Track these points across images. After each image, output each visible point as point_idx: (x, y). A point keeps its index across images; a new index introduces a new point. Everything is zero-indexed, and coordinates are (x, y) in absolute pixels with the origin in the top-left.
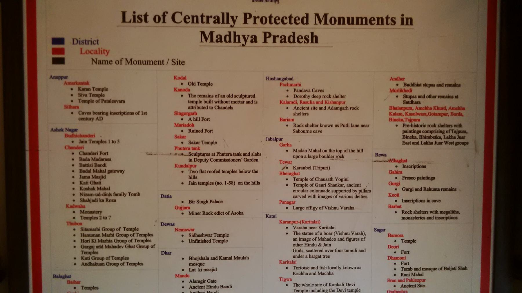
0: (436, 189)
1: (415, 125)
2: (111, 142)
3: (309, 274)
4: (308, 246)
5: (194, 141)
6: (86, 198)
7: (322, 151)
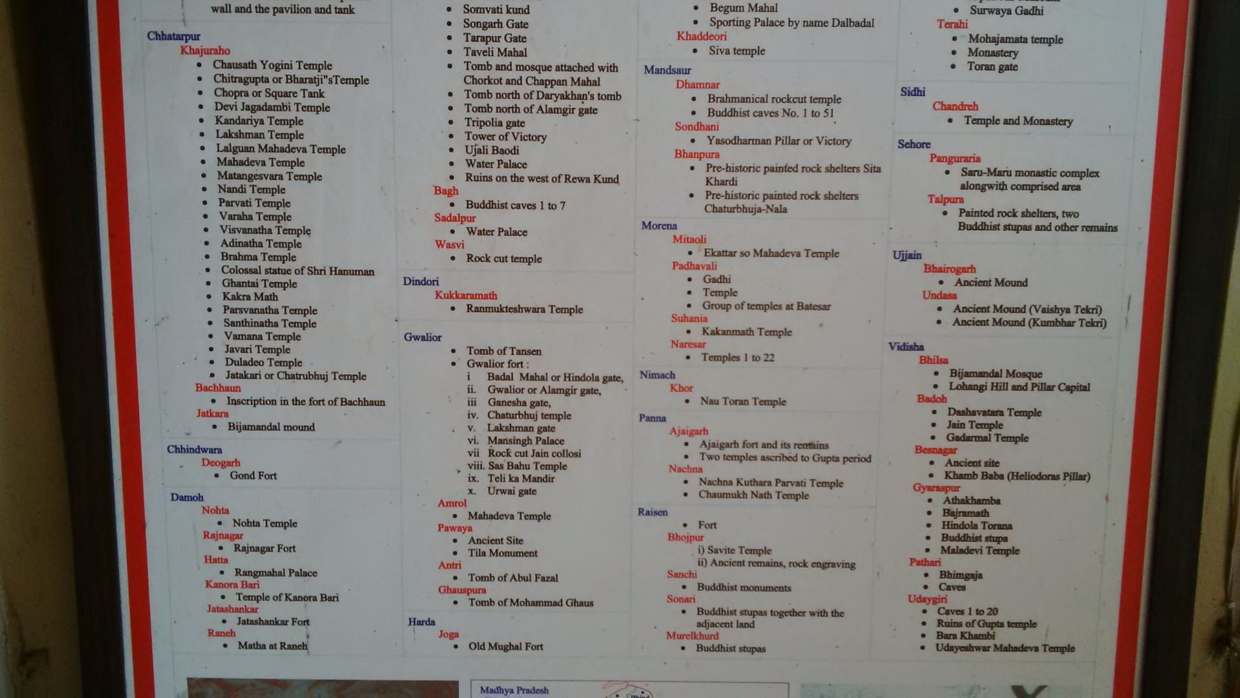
0: (239, 322)
4: (571, 379)
6: (240, 370)
7: (549, 378)
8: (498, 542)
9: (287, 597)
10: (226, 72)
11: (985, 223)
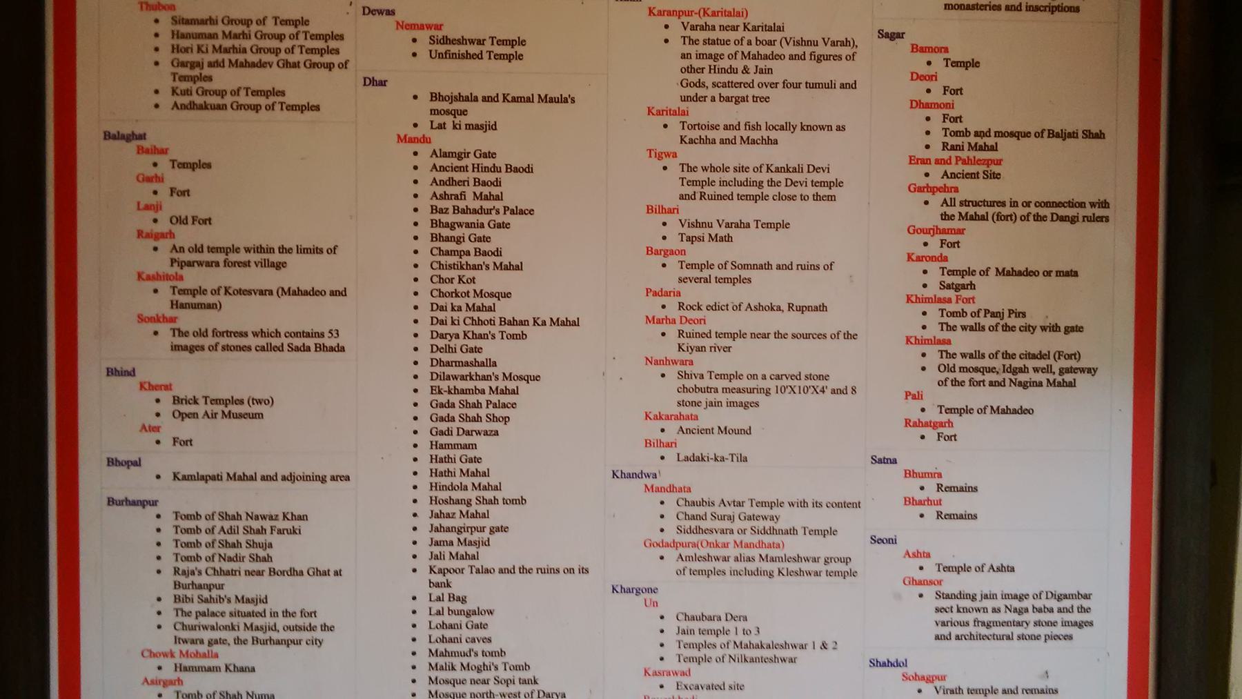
8: (462, 169)
9: (768, 168)
10: (443, 259)
11: (452, 178)
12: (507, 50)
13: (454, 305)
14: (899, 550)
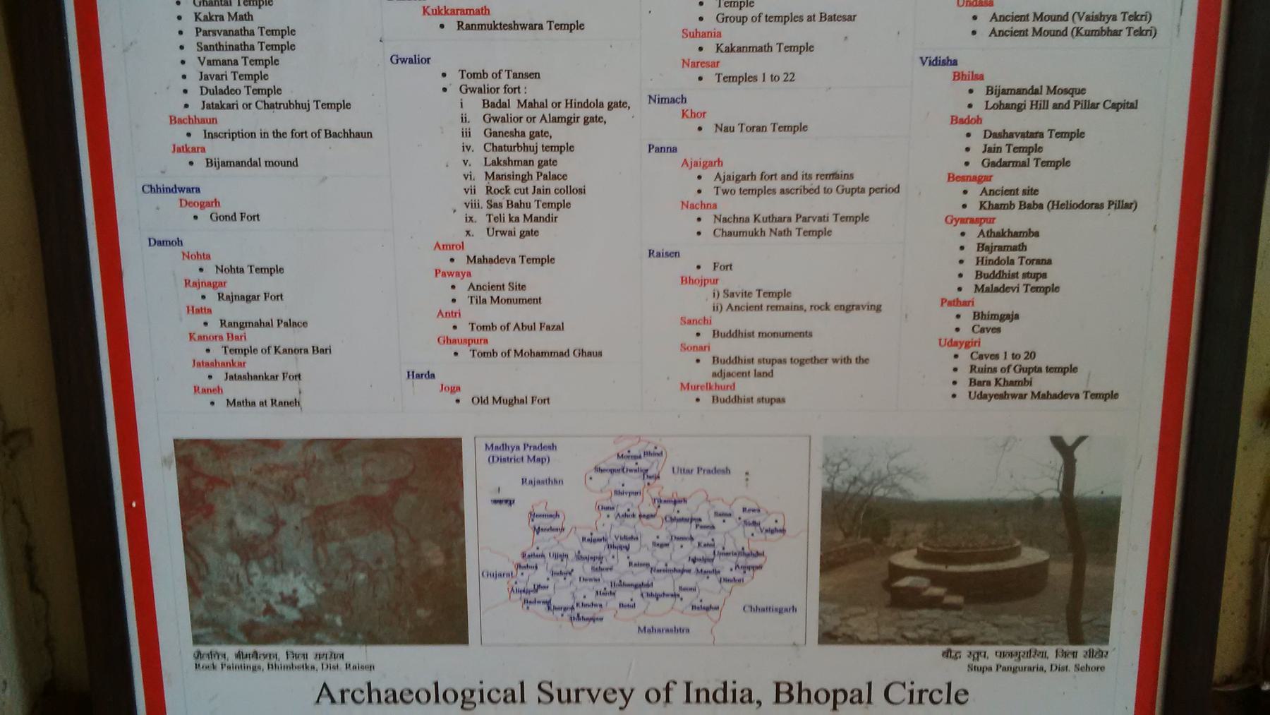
1: (1011, 273)
2: (768, 78)
3: (778, 191)
5: (498, 158)
12: (277, 40)
13: (500, 159)
14: (678, 158)
